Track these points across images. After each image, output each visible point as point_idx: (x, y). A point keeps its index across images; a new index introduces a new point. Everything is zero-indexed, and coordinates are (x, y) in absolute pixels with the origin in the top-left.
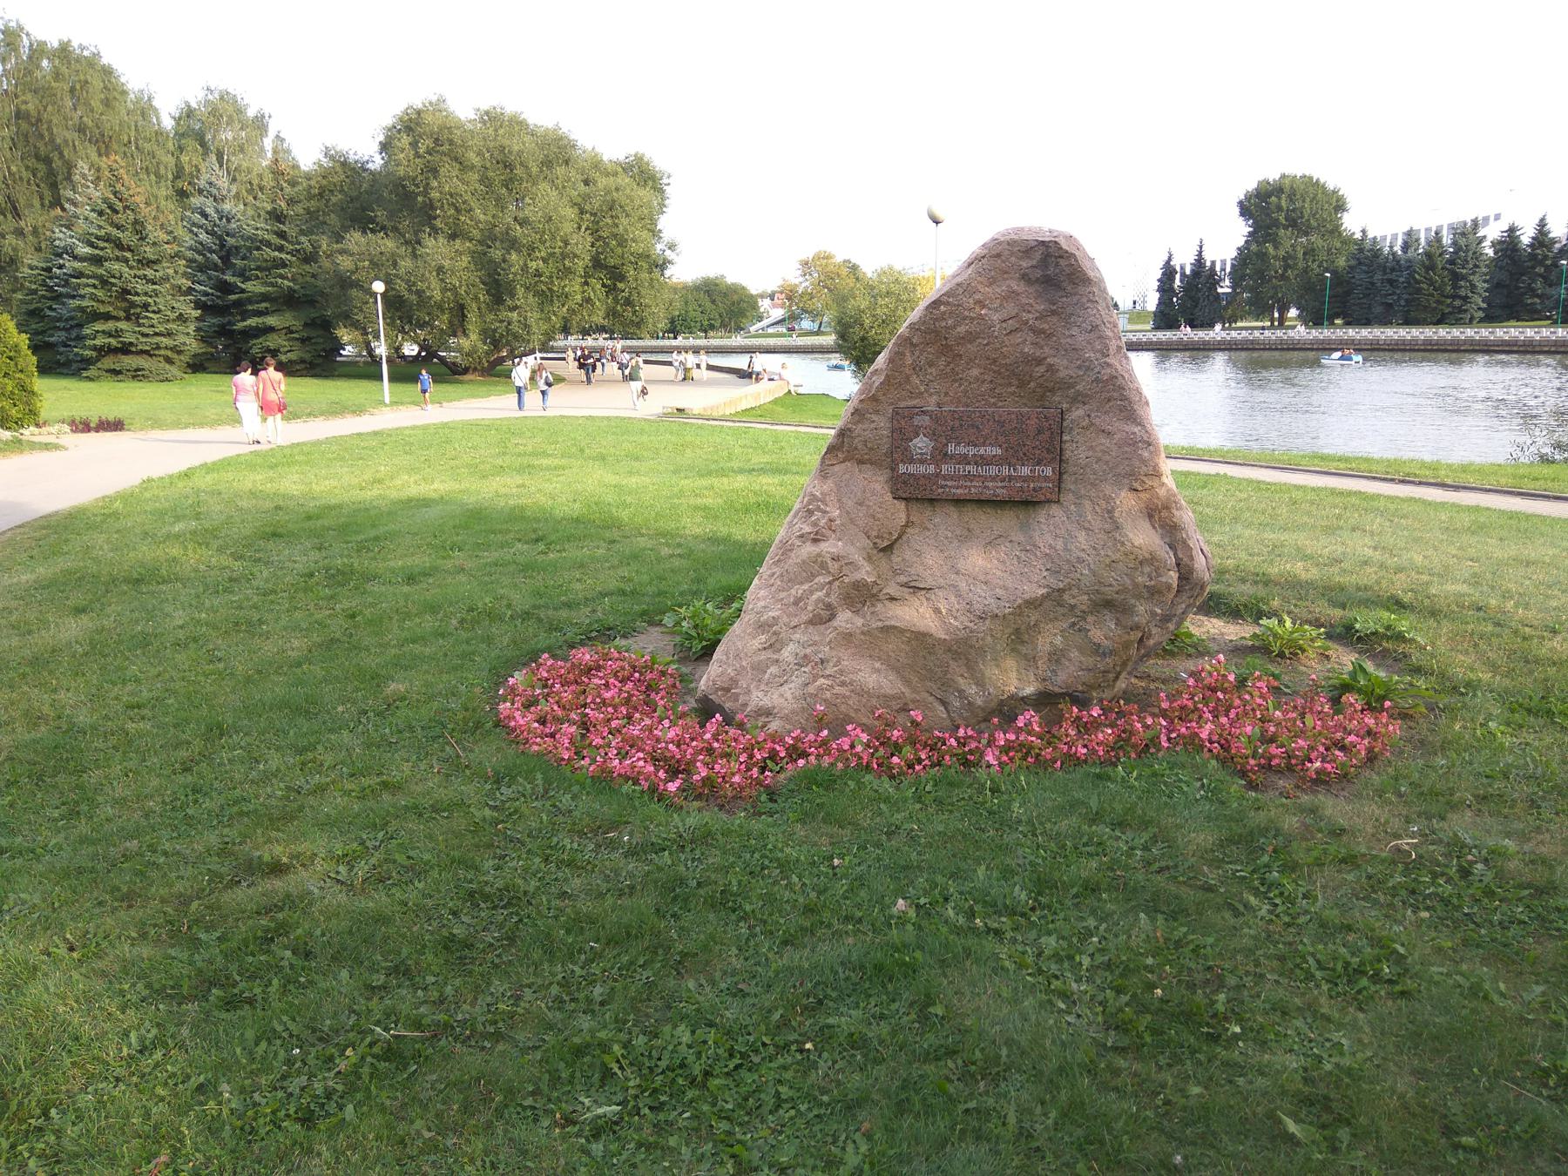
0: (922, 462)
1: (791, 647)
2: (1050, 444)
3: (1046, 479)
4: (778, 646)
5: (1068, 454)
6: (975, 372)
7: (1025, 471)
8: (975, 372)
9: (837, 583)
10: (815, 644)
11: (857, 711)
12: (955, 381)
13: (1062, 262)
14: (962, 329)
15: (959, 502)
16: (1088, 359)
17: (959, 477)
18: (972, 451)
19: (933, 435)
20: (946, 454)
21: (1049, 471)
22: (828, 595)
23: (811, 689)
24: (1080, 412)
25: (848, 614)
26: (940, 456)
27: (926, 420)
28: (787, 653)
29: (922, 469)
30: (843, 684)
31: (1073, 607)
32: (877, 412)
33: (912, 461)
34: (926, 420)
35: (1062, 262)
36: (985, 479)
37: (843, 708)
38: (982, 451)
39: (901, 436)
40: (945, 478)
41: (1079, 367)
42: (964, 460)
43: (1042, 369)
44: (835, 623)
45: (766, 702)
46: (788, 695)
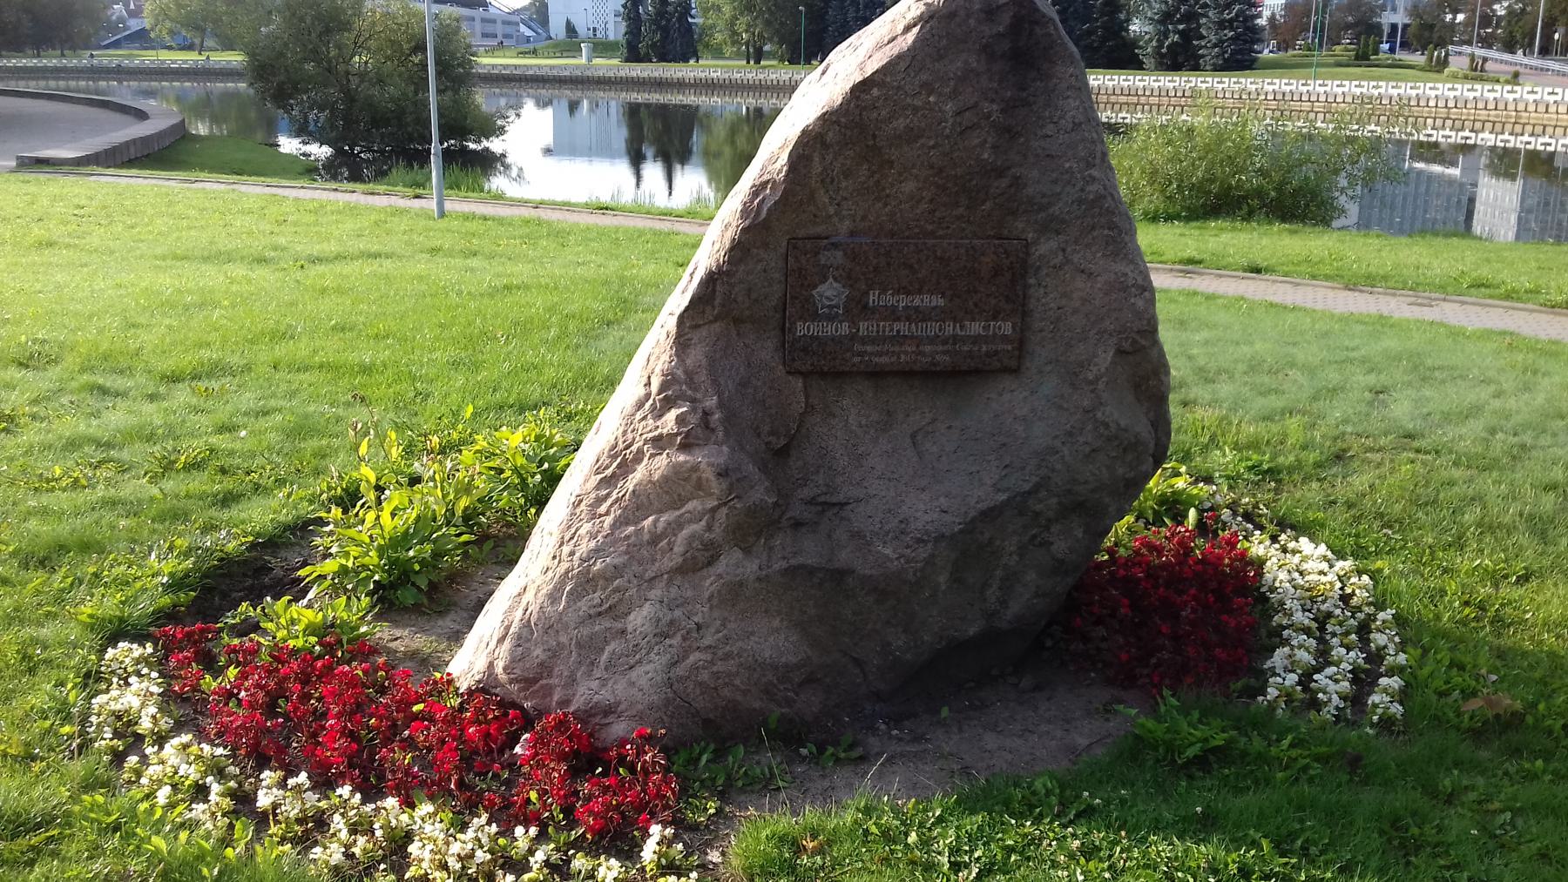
0: (831, 318)
1: (647, 609)
2: (1010, 283)
3: (1005, 338)
4: (622, 609)
5: (1032, 304)
6: (909, 186)
7: (975, 328)
8: (909, 186)
9: (724, 510)
10: (686, 602)
11: (745, 693)
12: (878, 199)
13: (1038, 30)
14: (900, 123)
15: (876, 375)
16: (1069, 171)
17: (884, 340)
18: (903, 302)
19: (849, 279)
20: (866, 307)
21: (1007, 328)
22: (709, 528)
23: (680, 671)
24: (1053, 244)
25: (737, 554)
26: (857, 308)
27: (838, 257)
28: (639, 619)
29: (830, 329)
30: (727, 657)
31: (1037, 514)
32: (766, 245)
33: (815, 317)
34: (838, 257)
35: (1038, 30)
36: (919, 341)
37: (726, 692)
38: (917, 302)
39: (799, 281)
40: (863, 341)
41: (1055, 182)
42: (893, 314)
43: (1004, 182)
44: (721, 566)
45: (605, 696)
46: (643, 682)
